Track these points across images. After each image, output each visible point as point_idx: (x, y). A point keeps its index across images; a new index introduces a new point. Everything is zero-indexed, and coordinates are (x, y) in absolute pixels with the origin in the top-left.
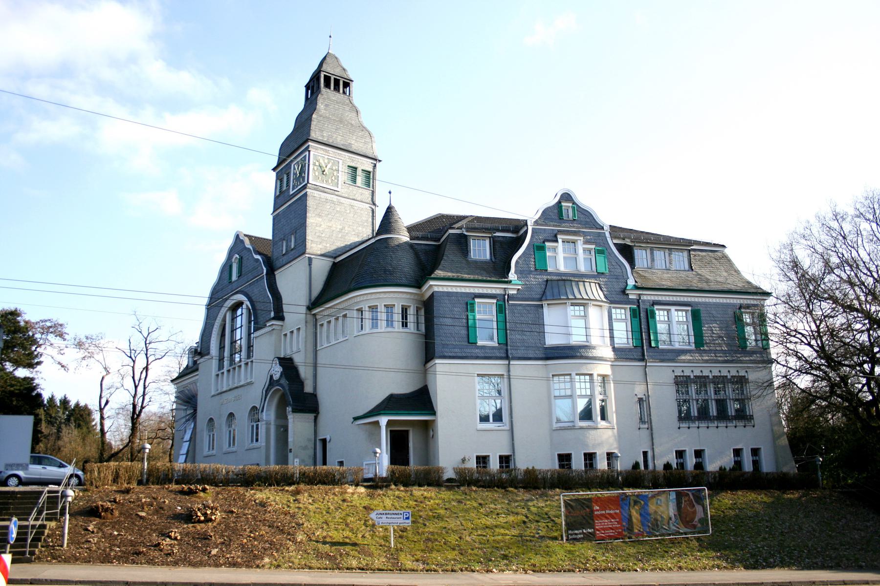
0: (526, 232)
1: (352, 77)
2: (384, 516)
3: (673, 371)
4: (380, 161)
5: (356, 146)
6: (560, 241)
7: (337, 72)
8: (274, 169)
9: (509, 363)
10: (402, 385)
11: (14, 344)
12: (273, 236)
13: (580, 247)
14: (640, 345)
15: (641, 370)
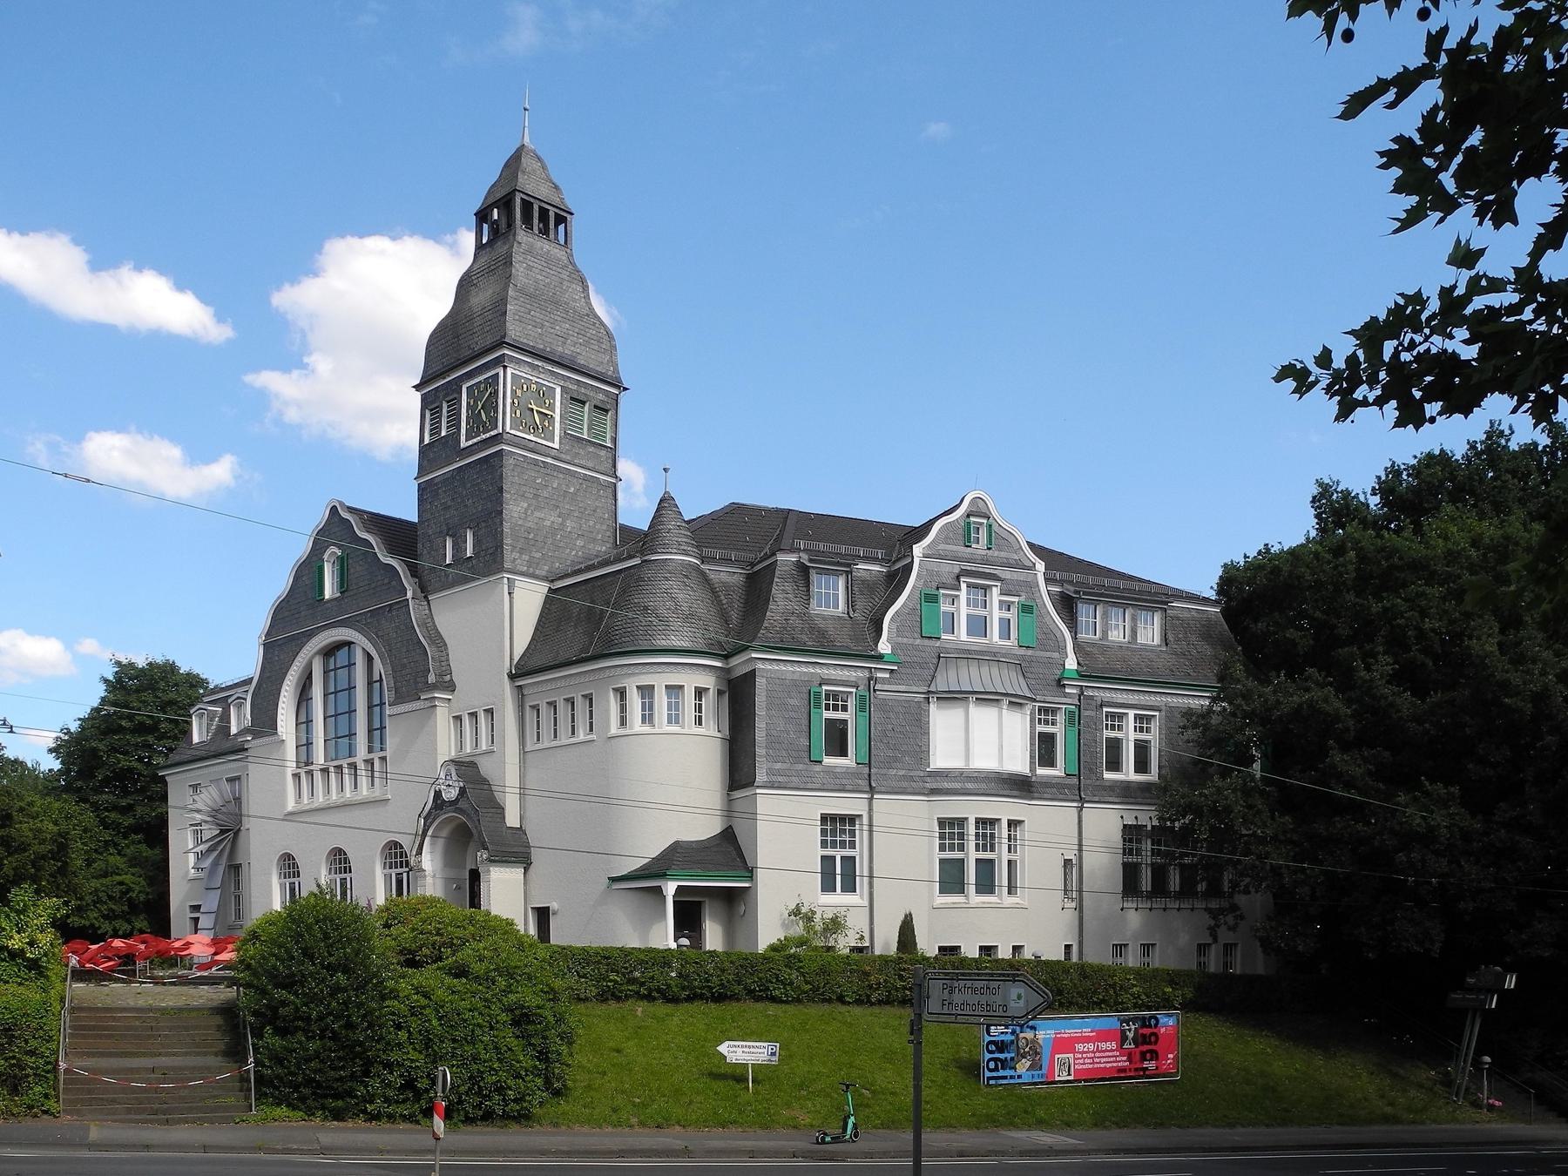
0: (909, 568)
1: (572, 207)
2: (739, 1050)
3: (1122, 817)
4: (625, 389)
5: (586, 358)
6: (963, 586)
7: (540, 190)
8: (417, 387)
9: (872, 796)
10: (703, 827)
13: (995, 595)
15: (1074, 812)
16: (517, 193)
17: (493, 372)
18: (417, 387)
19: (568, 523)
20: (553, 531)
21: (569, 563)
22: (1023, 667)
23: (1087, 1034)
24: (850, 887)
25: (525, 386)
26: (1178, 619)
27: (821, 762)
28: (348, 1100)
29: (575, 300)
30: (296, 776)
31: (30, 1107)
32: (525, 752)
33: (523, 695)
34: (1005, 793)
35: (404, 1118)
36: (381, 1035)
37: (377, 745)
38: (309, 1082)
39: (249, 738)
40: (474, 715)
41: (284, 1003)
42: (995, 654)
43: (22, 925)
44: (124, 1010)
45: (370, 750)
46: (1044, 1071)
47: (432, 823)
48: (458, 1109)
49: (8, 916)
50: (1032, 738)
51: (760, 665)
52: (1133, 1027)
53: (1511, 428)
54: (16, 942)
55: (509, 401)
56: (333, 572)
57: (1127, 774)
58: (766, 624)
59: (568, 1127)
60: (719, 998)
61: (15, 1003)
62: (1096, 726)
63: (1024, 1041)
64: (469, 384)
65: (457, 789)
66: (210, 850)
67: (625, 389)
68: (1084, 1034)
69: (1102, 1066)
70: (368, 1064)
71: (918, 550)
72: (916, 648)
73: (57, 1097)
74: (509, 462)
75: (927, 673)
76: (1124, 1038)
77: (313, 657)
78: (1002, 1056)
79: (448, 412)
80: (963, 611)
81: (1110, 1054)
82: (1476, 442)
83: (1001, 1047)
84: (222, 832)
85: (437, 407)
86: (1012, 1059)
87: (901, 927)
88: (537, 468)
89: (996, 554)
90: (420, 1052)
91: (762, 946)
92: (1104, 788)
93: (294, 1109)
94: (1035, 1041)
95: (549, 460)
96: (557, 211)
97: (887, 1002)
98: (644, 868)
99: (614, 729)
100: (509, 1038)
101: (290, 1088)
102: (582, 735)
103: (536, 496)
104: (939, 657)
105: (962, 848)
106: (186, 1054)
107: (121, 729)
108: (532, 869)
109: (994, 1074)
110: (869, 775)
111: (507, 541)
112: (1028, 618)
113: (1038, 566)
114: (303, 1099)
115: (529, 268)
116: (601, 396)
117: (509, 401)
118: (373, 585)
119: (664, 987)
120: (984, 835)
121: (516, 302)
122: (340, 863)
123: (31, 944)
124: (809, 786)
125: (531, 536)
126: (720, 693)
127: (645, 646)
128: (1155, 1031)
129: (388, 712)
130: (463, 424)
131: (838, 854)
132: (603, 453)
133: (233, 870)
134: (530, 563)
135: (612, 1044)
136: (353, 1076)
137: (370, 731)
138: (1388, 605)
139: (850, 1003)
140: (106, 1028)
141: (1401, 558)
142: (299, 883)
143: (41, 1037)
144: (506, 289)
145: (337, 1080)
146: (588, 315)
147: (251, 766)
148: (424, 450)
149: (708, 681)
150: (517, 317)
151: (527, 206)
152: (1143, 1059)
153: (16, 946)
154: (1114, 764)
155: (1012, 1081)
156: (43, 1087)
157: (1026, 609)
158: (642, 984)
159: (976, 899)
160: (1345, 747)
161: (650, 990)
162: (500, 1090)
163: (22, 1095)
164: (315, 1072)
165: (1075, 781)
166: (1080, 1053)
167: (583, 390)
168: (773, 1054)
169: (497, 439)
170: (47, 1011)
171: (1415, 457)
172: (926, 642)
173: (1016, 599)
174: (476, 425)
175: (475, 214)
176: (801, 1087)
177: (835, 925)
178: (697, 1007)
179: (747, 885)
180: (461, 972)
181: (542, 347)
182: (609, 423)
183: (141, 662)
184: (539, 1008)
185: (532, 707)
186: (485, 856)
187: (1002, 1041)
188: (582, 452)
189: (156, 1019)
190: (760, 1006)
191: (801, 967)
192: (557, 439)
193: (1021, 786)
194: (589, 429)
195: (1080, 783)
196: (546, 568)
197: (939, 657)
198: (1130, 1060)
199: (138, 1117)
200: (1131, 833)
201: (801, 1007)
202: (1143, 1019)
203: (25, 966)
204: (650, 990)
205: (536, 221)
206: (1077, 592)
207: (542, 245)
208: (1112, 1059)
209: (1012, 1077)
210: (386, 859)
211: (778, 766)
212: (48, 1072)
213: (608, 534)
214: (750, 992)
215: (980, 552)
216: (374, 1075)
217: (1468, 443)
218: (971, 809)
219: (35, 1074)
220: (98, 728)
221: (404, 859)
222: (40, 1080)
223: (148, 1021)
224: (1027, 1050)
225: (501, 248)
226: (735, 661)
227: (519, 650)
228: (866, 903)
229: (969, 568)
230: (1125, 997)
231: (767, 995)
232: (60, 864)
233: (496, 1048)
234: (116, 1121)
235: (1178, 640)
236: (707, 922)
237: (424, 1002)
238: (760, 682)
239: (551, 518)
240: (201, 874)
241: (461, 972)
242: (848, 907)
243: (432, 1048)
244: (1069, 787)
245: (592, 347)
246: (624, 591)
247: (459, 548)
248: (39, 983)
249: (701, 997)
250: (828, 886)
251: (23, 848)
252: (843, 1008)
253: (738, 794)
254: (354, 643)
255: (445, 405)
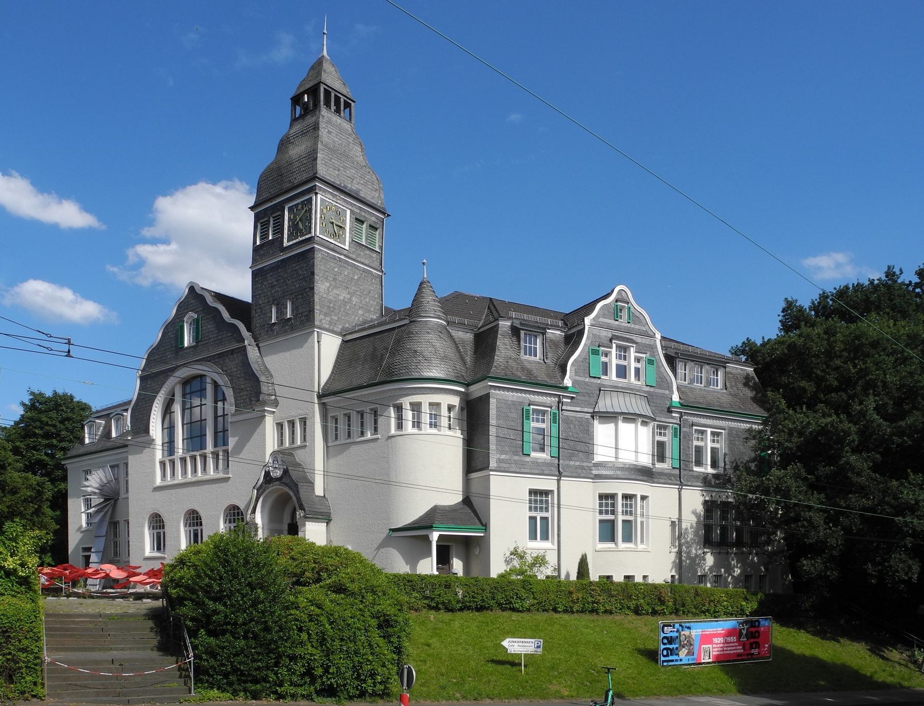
2: (516, 644)
4: (388, 215)
6: (614, 345)
8: (252, 208)
11: (232, 442)
12: (254, 296)
14: (678, 467)
16: (321, 84)
17: (307, 197)
18: (252, 208)
19: (354, 299)
20: (345, 303)
21: (354, 324)
22: (649, 398)
23: (720, 632)
24: (545, 537)
25: (328, 207)
26: (731, 373)
27: (529, 455)
28: (264, 684)
29: (357, 156)
30: (163, 464)
31: (23, 693)
32: (327, 447)
33: (326, 409)
34: (633, 477)
35: (303, 696)
36: (290, 635)
37: (220, 441)
38: (235, 670)
39: (129, 438)
40: (292, 423)
41: (215, 612)
42: (632, 390)
43: (14, 550)
44: (81, 616)
45: (215, 445)
46: (695, 656)
47: (262, 493)
48: (341, 690)
49: (4, 544)
50: (653, 444)
51: (492, 391)
52: (746, 627)
53: (901, 270)
54: (10, 563)
55: (319, 216)
56: (190, 329)
57: (706, 469)
58: (495, 364)
59: (417, 701)
60: (480, 609)
61: (10, 612)
62: (689, 437)
63: (684, 636)
64: (290, 205)
65: (282, 470)
66: (97, 512)
67: (388, 215)
68: (718, 632)
69: (728, 652)
70: (279, 657)
71: (588, 321)
72: (586, 383)
73: (43, 684)
74: (318, 256)
75: (593, 400)
76: (740, 634)
77: (176, 384)
78: (671, 647)
79: (274, 224)
80: (614, 362)
81: (733, 644)
82: (874, 280)
83: (671, 640)
84: (106, 500)
85: (267, 221)
86: (677, 648)
87: (579, 563)
88: (335, 261)
89: (633, 326)
90: (316, 648)
91: (494, 574)
92: (693, 477)
93: (223, 692)
94: (690, 637)
95: (342, 257)
96: (345, 99)
97: (582, 611)
98: (414, 522)
99: (393, 431)
100: (376, 637)
101: (221, 675)
102: (369, 435)
103: (334, 279)
104: (600, 390)
105: (613, 512)
106: (131, 649)
107: (35, 435)
108: (331, 523)
109: (666, 659)
110: (559, 465)
111: (317, 307)
112: (650, 367)
113: (657, 335)
114: (230, 684)
115: (329, 132)
116: (374, 219)
117: (319, 216)
118: (220, 337)
119: (447, 601)
120: (626, 505)
121: (323, 152)
122: (193, 520)
123: (22, 565)
124: (522, 470)
125: (331, 305)
126: (462, 409)
127: (416, 375)
128: (758, 629)
129: (230, 420)
130: (286, 231)
131: (539, 515)
132: (374, 255)
133: (112, 525)
134: (330, 323)
135: (422, 640)
136: (268, 668)
137: (216, 433)
138: (863, 367)
139: (560, 612)
140: (67, 630)
141: (867, 339)
142: (164, 533)
143: (31, 638)
144: (316, 144)
145: (256, 669)
146: (365, 166)
147: (130, 457)
148: (256, 249)
149: (455, 401)
150: (324, 162)
151: (327, 94)
152: (752, 648)
153: (11, 567)
154: (699, 463)
155: (676, 663)
156: (33, 677)
157: (650, 362)
158: (433, 599)
159: (622, 545)
160: (855, 451)
161: (438, 603)
162: (373, 675)
163: (16, 683)
164: (240, 663)
165: (677, 472)
166: (715, 644)
167: (363, 214)
168: (539, 647)
169: (310, 240)
170: (36, 617)
171: (835, 289)
172: (592, 380)
173: (644, 356)
174: (295, 230)
175: (291, 99)
176: (553, 668)
177: (540, 561)
178: (466, 613)
179: (482, 535)
180: (339, 589)
181: (338, 183)
182: (377, 236)
183: (49, 393)
184: (395, 616)
185: (332, 417)
186: (302, 515)
187: (671, 637)
188: (362, 253)
189: (105, 622)
190: (506, 614)
191: (531, 588)
192: (347, 243)
193: (646, 474)
194: (366, 239)
195: (680, 474)
196: (341, 327)
197: (600, 390)
198: (744, 648)
199: (104, 699)
200: (709, 506)
201: (530, 615)
202: (751, 622)
203: (17, 582)
204: (438, 603)
205: (333, 104)
206: (676, 353)
207: (336, 119)
208: (733, 648)
209: (677, 660)
210: (227, 517)
211: (503, 457)
212: (36, 665)
213: (378, 308)
214: (500, 605)
215: (623, 324)
216: (283, 666)
217: (869, 280)
218: (620, 488)
219: (26, 667)
220: (20, 434)
221: (199, 521)
222: (30, 672)
223: (99, 624)
224: (685, 642)
225: (310, 120)
226: (473, 388)
227: (324, 379)
228: (556, 547)
229: (617, 334)
230: (719, 608)
231: (510, 606)
232: (36, 506)
233: (370, 645)
234: (89, 702)
235: (732, 386)
236: (454, 559)
237: (318, 611)
238: (493, 402)
239: (343, 295)
240: (91, 528)
241: (339, 589)
242: (546, 550)
243: (326, 645)
244: (674, 475)
245: (369, 186)
246: (398, 341)
247: (281, 312)
248: (28, 596)
249: (469, 608)
250: (533, 536)
251: (14, 492)
252: (557, 616)
253: (474, 475)
254: (206, 376)
255: (272, 220)
